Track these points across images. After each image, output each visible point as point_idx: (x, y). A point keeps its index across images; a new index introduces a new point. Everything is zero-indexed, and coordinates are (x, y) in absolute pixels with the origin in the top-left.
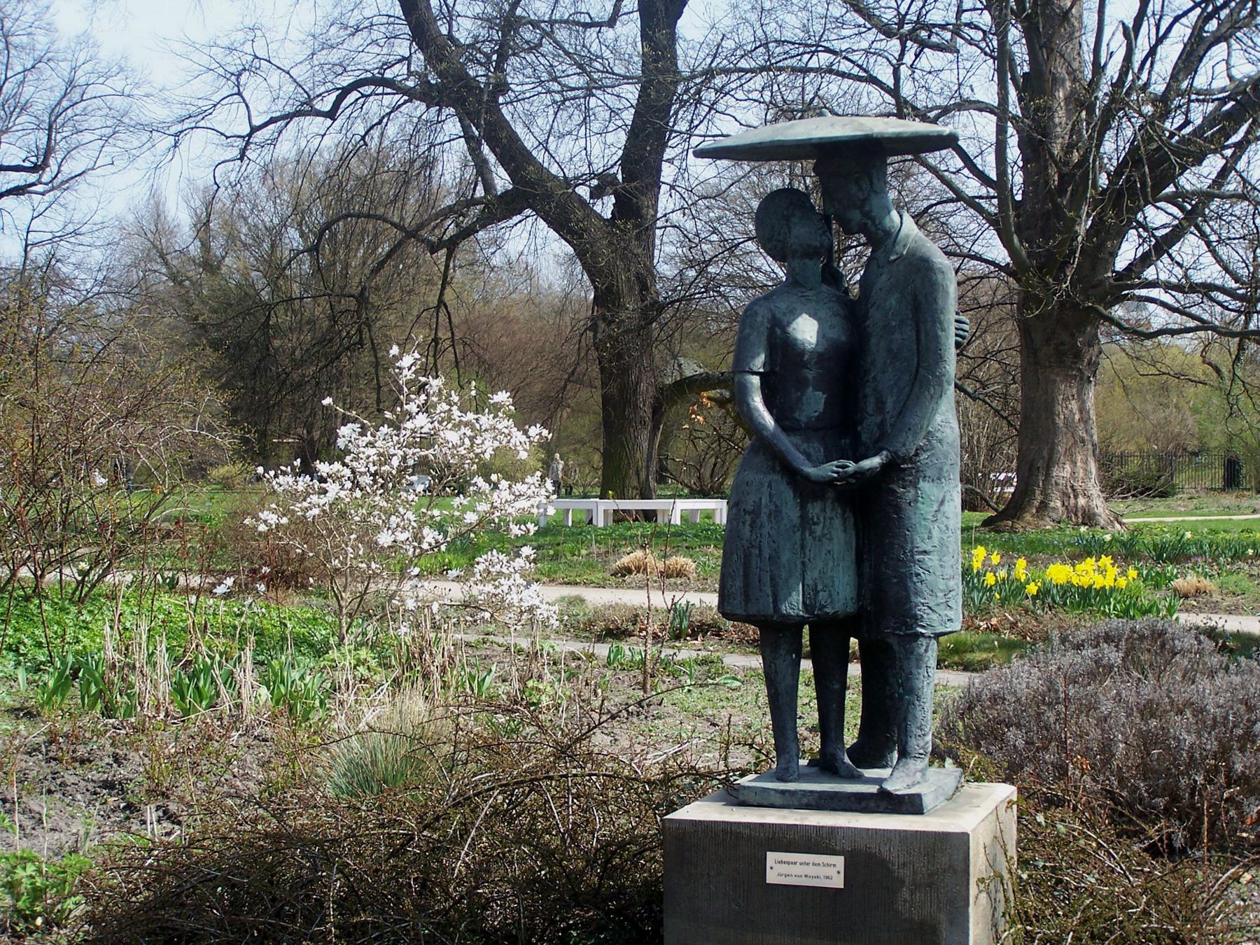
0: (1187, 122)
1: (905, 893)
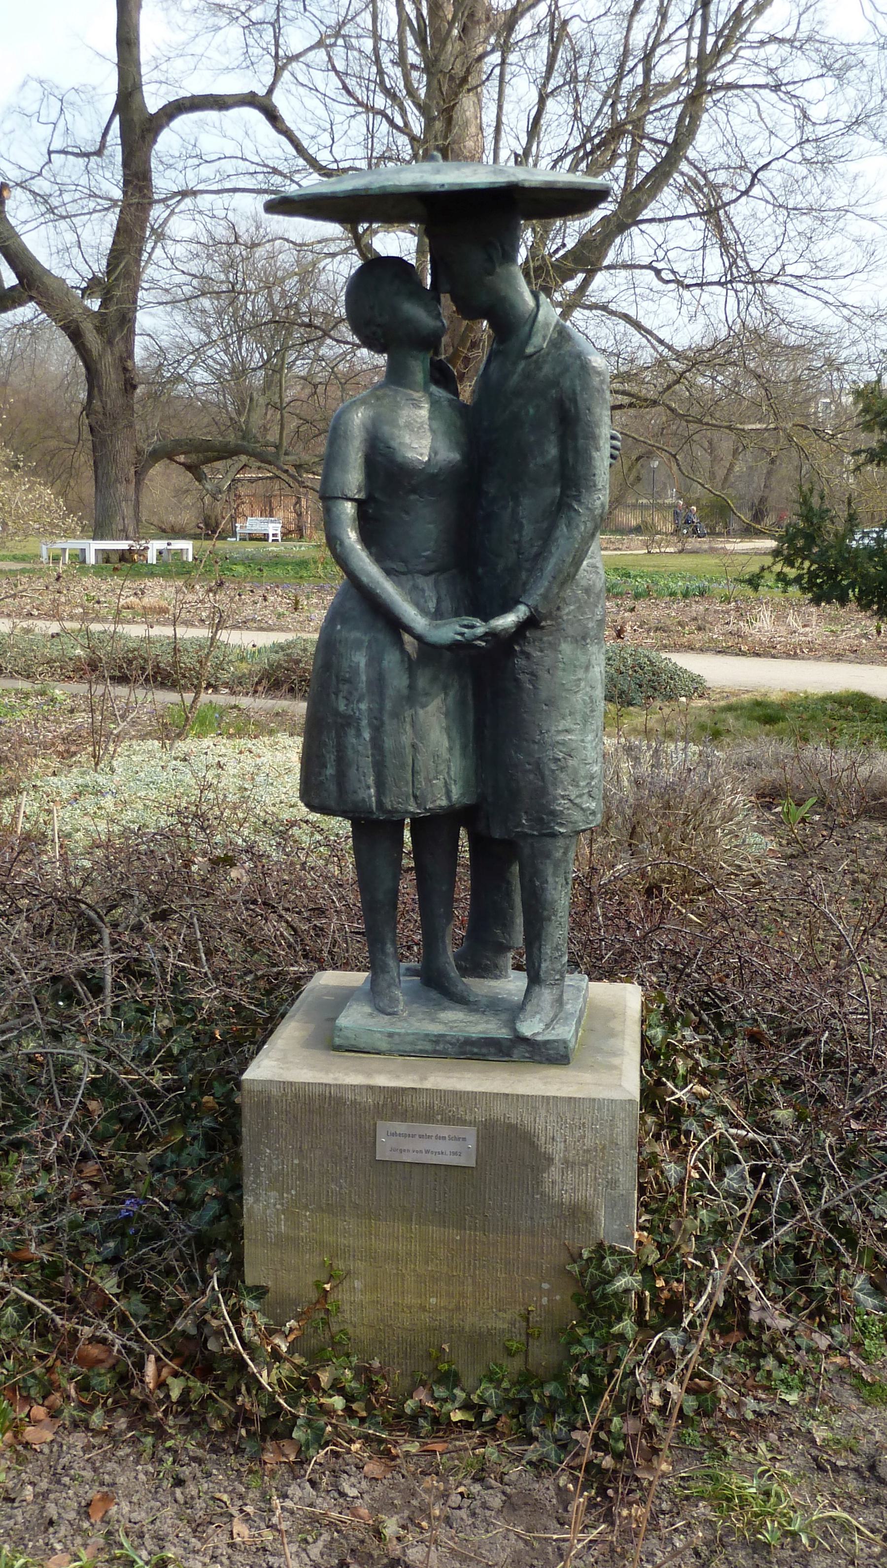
0: (564, 245)
1: (554, 1173)
